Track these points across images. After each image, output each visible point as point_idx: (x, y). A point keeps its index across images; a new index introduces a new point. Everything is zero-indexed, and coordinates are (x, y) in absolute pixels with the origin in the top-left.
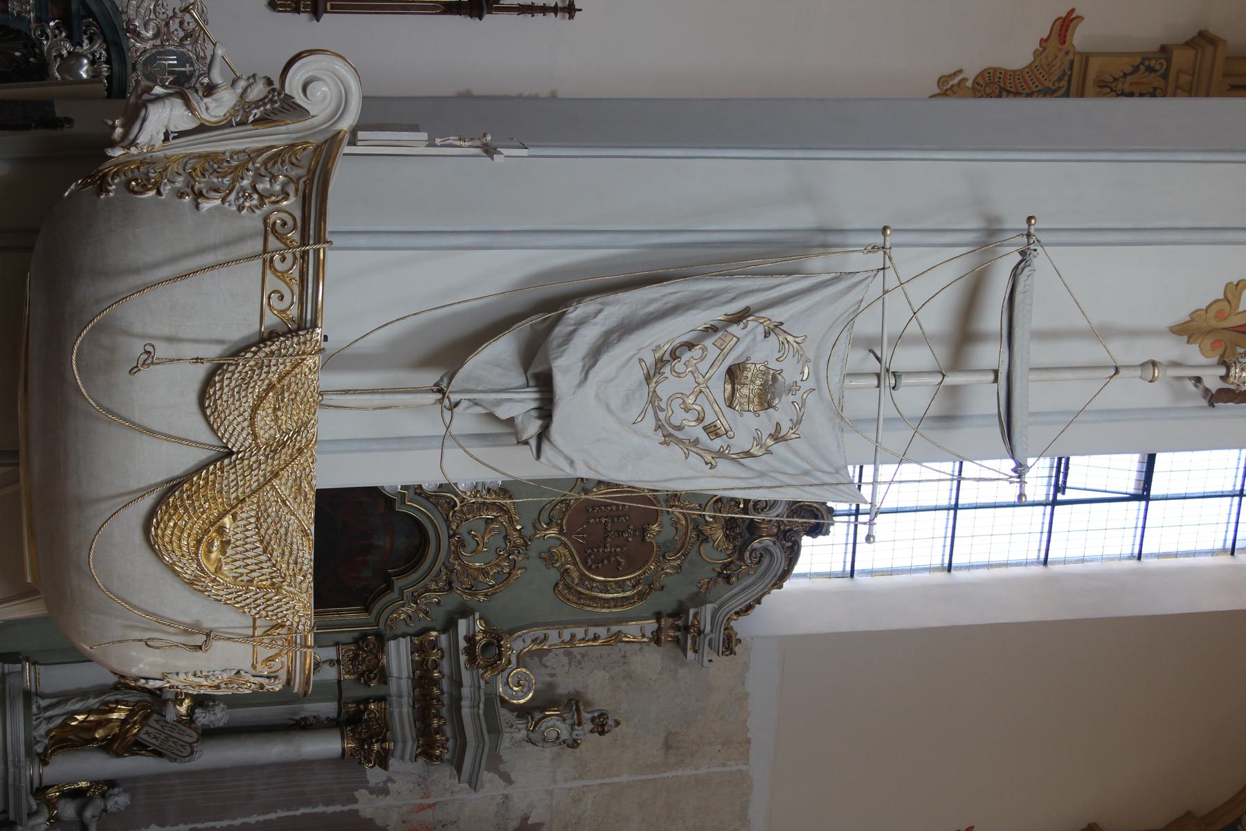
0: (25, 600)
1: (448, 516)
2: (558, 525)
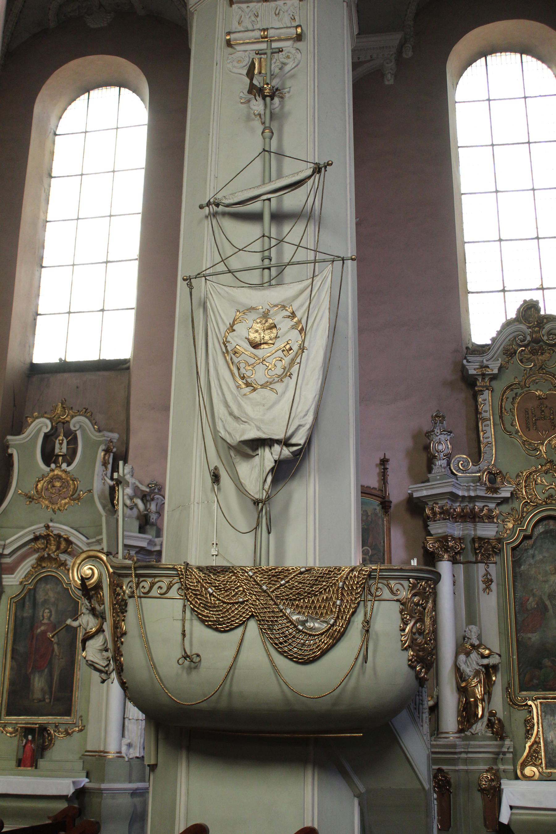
0: (398, 738)
1: (533, 506)
2: (538, 446)
